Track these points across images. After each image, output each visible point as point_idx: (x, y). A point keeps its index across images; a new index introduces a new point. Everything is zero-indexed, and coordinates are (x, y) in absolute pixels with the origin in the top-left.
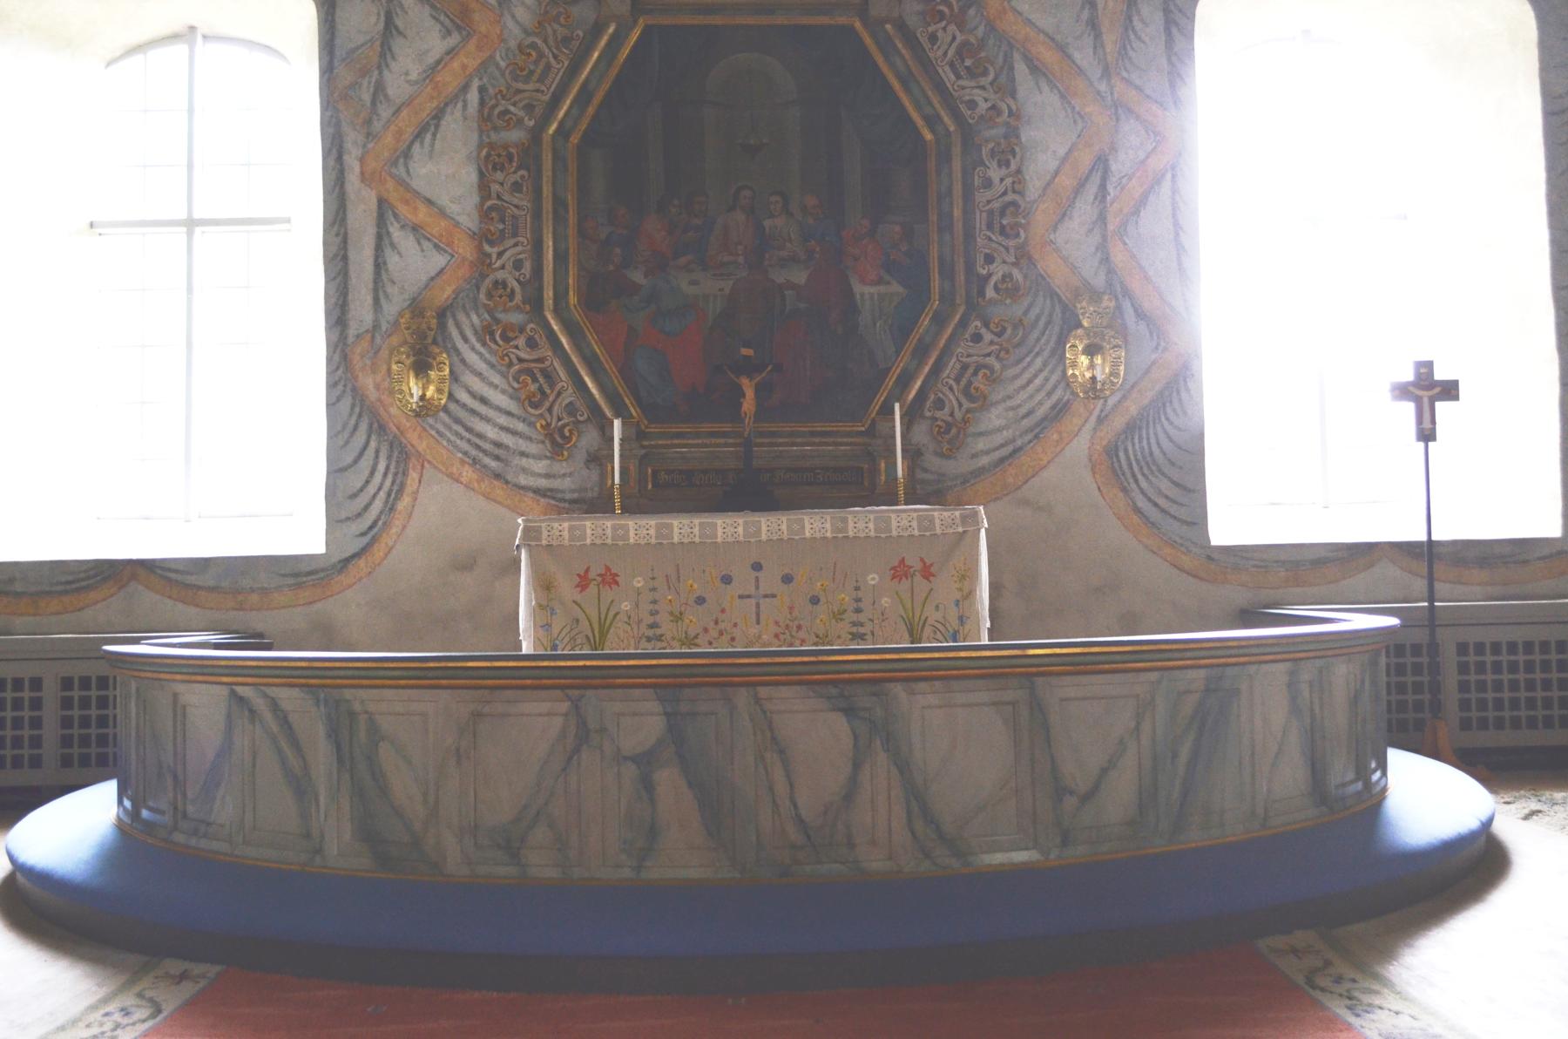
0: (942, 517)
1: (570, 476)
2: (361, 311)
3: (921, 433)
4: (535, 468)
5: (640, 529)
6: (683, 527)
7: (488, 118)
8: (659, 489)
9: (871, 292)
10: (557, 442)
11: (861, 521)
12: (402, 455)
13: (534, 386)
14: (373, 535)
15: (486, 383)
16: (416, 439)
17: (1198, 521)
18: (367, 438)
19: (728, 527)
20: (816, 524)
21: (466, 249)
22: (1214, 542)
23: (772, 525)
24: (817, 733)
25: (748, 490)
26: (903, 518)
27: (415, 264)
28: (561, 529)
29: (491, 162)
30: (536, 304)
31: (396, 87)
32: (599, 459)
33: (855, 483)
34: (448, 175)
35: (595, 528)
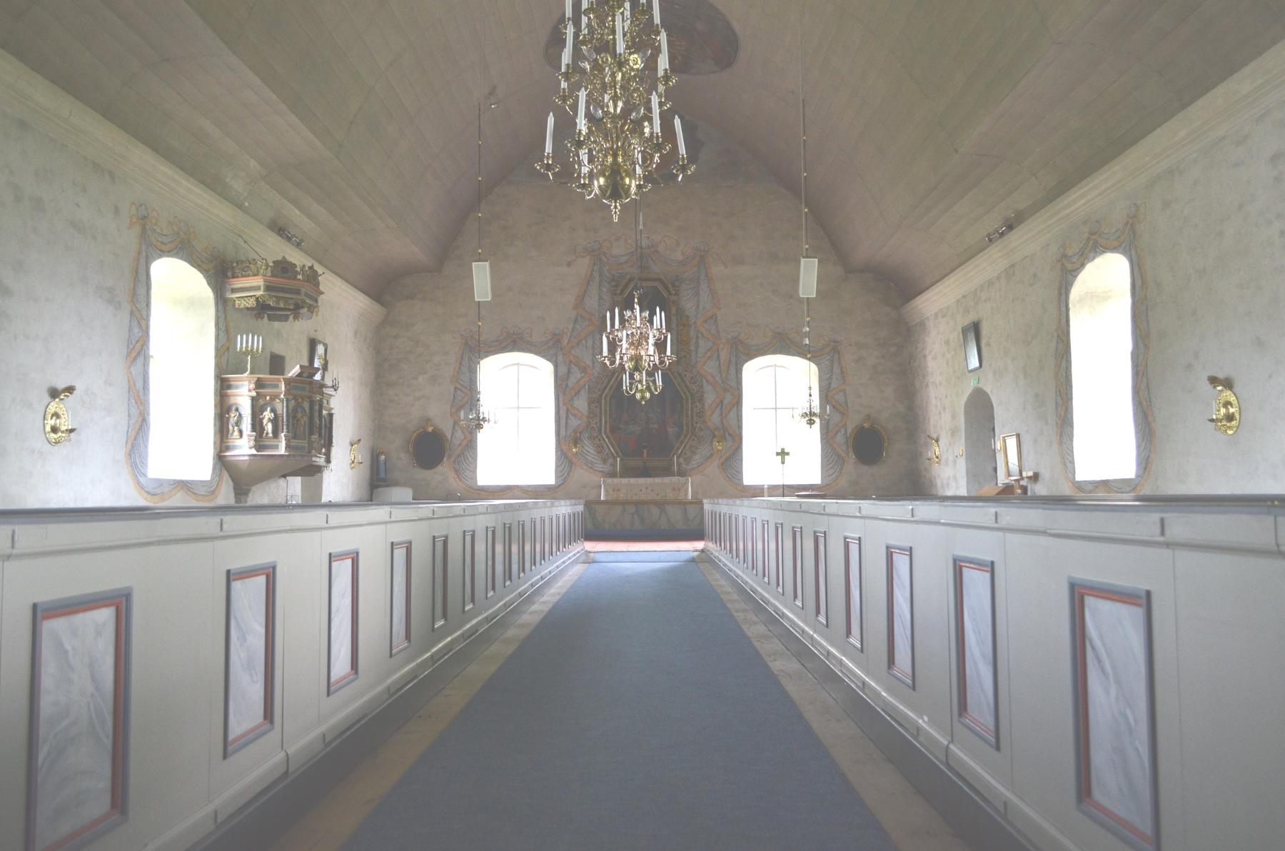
0: (682, 479)
1: (607, 468)
2: (563, 432)
3: (681, 460)
4: (600, 466)
5: (625, 481)
6: (633, 480)
7: (590, 391)
8: (628, 472)
9: (671, 430)
10: (604, 461)
11: (666, 480)
12: (571, 463)
13: (600, 449)
14: (565, 480)
15: (589, 448)
16: (574, 460)
17: (741, 479)
18: (565, 460)
19: (641, 481)
20: (658, 480)
21: (585, 419)
22: (208, 477)
23: (649, 480)
24: (655, 511)
25: (645, 473)
26: (675, 479)
27: (574, 423)
28: (610, 480)
29: (590, 402)
30: (600, 431)
31: (570, 384)
32: (614, 465)
33: (667, 471)
34: (582, 404)
35: (616, 480)
